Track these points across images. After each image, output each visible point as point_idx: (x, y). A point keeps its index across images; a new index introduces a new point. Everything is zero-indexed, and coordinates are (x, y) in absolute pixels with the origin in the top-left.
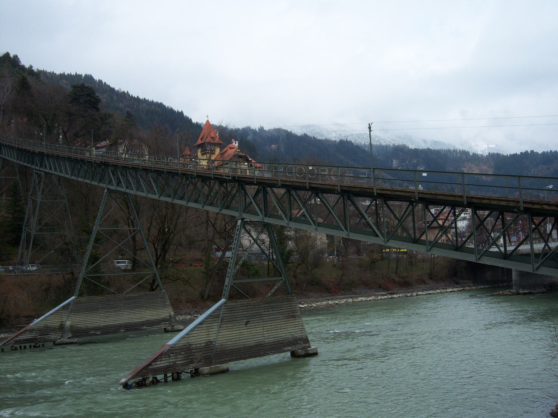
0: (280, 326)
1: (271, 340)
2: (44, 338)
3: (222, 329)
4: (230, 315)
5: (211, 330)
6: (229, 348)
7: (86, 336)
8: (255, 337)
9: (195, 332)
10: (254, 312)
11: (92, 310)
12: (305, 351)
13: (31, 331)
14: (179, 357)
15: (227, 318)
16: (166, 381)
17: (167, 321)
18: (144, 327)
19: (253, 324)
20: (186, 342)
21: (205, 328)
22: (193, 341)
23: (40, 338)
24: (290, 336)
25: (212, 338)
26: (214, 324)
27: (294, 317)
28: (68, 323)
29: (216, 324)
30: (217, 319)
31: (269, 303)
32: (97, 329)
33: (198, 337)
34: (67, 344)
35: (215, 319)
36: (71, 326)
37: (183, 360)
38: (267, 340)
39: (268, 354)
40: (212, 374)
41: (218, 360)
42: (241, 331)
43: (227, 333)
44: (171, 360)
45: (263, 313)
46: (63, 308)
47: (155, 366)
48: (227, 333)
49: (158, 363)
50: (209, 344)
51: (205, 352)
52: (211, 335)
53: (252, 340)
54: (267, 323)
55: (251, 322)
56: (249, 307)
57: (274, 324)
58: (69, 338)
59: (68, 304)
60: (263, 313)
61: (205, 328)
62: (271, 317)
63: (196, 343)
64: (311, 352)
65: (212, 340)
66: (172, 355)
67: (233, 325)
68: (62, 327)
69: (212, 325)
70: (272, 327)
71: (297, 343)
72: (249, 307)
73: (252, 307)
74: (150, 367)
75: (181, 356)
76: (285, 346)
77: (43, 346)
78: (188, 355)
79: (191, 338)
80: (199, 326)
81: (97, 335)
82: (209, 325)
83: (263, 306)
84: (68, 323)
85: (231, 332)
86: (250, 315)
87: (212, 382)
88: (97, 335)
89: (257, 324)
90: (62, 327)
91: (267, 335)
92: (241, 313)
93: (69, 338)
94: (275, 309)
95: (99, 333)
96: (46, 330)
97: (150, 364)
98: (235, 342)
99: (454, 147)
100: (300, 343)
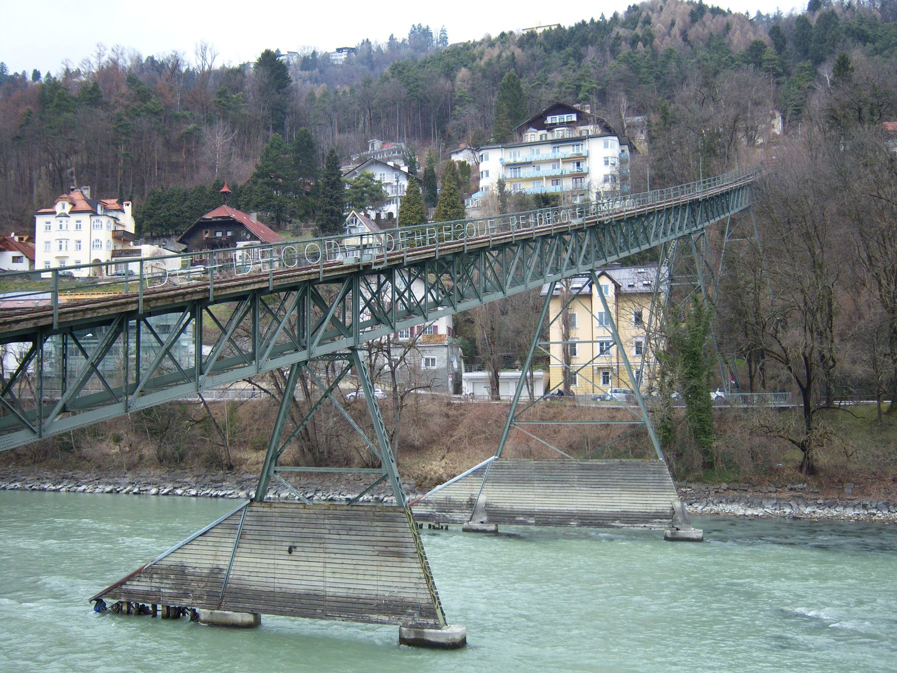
0: (364, 567)
1: (342, 592)
2: (444, 516)
3: (242, 550)
4: (259, 528)
5: (220, 549)
6: (253, 588)
7: (511, 523)
8: (305, 578)
9: (194, 547)
10: (305, 530)
11: (523, 480)
12: (416, 633)
13: (427, 503)
14: (166, 581)
15: (252, 532)
16: (154, 615)
17: (666, 517)
18: (617, 523)
19: (303, 554)
20: (178, 560)
21: (210, 544)
22: (189, 561)
23: (439, 516)
24: (387, 594)
25: (223, 563)
26: (227, 540)
27: (399, 555)
28: (482, 499)
29: (231, 540)
30: (233, 531)
31: (340, 519)
32: (530, 514)
33: (199, 557)
34: (477, 531)
35: (229, 531)
36: (487, 504)
37: (171, 588)
38: (331, 590)
39: (333, 617)
40: (214, 624)
41: (232, 604)
42: (277, 562)
43: (252, 560)
44: (153, 584)
45: (327, 536)
46: (475, 473)
47: (130, 587)
48: (252, 560)
49: (135, 583)
50: (216, 571)
51: (209, 584)
52: (221, 558)
53: (298, 582)
54: (333, 556)
55: (298, 549)
56: (296, 520)
57: (350, 562)
58: (482, 522)
59: (483, 468)
60: (327, 536)
61: (210, 544)
62: (343, 547)
63: (194, 565)
64: (431, 639)
65: (221, 567)
66: (155, 576)
67: (263, 547)
68: (471, 504)
69: (223, 540)
70: (345, 566)
71: (403, 613)
72: (296, 520)
73: (303, 520)
74: (124, 587)
75: (169, 582)
76: (372, 611)
77: (447, 529)
78: (180, 582)
79: (186, 556)
80: (200, 538)
81: (530, 524)
82: (218, 539)
83: (326, 521)
84: (482, 499)
85: (259, 560)
86: (299, 535)
87: (206, 636)
88: (530, 524)
89: (311, 554)
90: (471, 504)
91: (332, 580)
92: (280, 529)
93: (482, 522)
94: (354, 533)
95: (532, 521)
96: (448, 505)
97: (122, 583)
98: (265, 580)
99: (134, 50)
100: (410, 614)
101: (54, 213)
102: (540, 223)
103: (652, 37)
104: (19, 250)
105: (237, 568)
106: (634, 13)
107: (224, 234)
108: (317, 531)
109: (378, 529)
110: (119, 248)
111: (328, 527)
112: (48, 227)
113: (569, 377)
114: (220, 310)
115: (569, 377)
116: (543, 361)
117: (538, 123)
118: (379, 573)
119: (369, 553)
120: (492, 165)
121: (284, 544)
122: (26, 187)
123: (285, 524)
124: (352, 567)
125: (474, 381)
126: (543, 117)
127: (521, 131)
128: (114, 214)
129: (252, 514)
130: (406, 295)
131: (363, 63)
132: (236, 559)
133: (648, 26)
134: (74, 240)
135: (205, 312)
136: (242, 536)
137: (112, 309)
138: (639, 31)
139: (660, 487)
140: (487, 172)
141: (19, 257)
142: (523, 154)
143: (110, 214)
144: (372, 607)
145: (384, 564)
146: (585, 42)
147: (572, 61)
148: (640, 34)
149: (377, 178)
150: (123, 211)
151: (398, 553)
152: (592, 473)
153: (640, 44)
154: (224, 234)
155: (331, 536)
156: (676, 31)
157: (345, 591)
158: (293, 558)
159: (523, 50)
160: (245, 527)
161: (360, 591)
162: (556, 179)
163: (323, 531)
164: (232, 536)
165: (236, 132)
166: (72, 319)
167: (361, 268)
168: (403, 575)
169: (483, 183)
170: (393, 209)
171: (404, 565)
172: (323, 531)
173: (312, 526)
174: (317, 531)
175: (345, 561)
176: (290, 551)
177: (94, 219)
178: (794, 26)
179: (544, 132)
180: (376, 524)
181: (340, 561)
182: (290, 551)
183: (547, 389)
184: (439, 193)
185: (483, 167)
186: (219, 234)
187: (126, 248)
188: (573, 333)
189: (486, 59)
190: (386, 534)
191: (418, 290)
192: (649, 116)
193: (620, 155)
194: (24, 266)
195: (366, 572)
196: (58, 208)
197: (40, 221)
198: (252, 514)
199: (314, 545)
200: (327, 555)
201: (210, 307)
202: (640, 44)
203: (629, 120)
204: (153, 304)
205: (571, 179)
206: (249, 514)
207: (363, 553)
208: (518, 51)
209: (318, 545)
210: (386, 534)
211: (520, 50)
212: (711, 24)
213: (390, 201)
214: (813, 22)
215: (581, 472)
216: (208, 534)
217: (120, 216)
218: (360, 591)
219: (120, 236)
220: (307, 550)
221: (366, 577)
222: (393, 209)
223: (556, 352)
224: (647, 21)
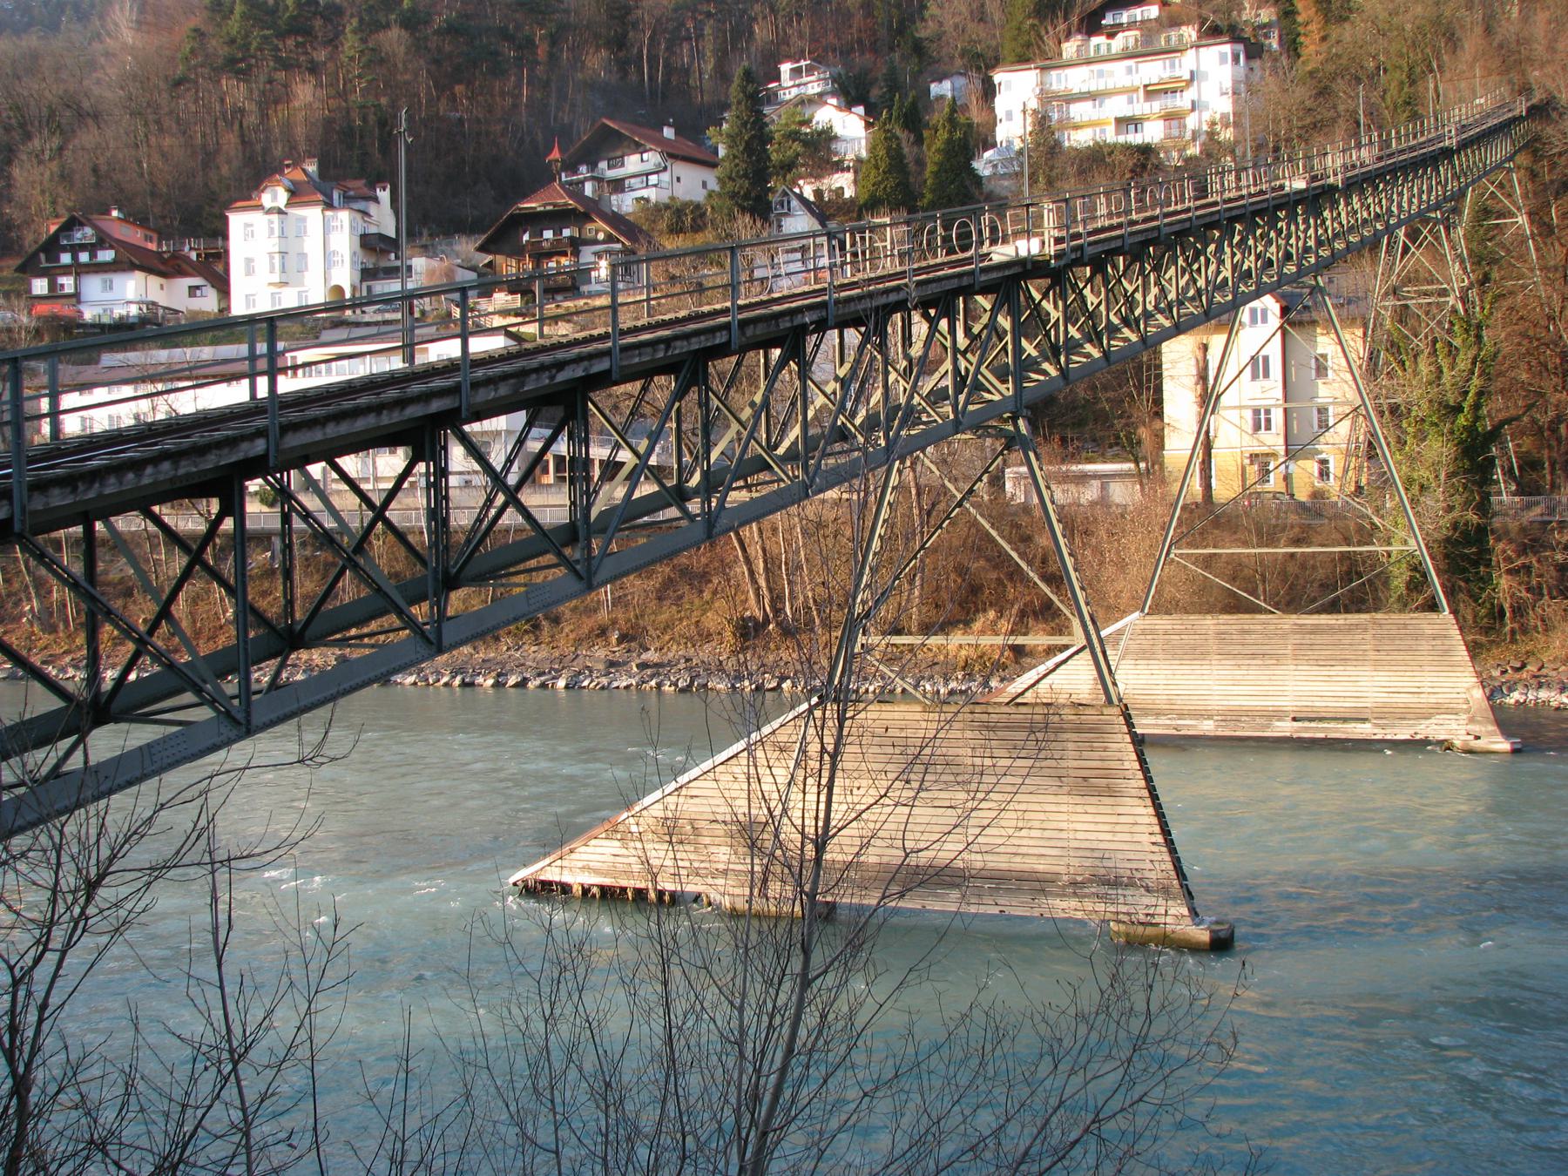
0: (1042, 816)
9: (938, 828)
101: (260, 207)
107: (558, 232)
118: (1072, 826)
126: (1099, 14)
128: (361, 205)
137: (694, 340)
139: (1443, 657)
141: (198, 287)
143: (357, 206)
145: (1079, 809)
150: (376, 200)
152: (1318, 639)
154: (558, 232)
162: (1123, 123)
166: (637, 360)
167: (1029, 267)
168: (1118, 828)
171: (1121, 810)
177: (329, 213)
186: (548, 234)
187: (383, 264)
193: (1247, 76)
194: (208, 302)
195: (1045, 825)
196: (267, 199)
197: (237, 221)
204: (749, 331)
205: (1161, 122)
213: (839, 167)
217: (373, 208)
219: (370, 243)
221: (1047, 834)
222: (844, 183)
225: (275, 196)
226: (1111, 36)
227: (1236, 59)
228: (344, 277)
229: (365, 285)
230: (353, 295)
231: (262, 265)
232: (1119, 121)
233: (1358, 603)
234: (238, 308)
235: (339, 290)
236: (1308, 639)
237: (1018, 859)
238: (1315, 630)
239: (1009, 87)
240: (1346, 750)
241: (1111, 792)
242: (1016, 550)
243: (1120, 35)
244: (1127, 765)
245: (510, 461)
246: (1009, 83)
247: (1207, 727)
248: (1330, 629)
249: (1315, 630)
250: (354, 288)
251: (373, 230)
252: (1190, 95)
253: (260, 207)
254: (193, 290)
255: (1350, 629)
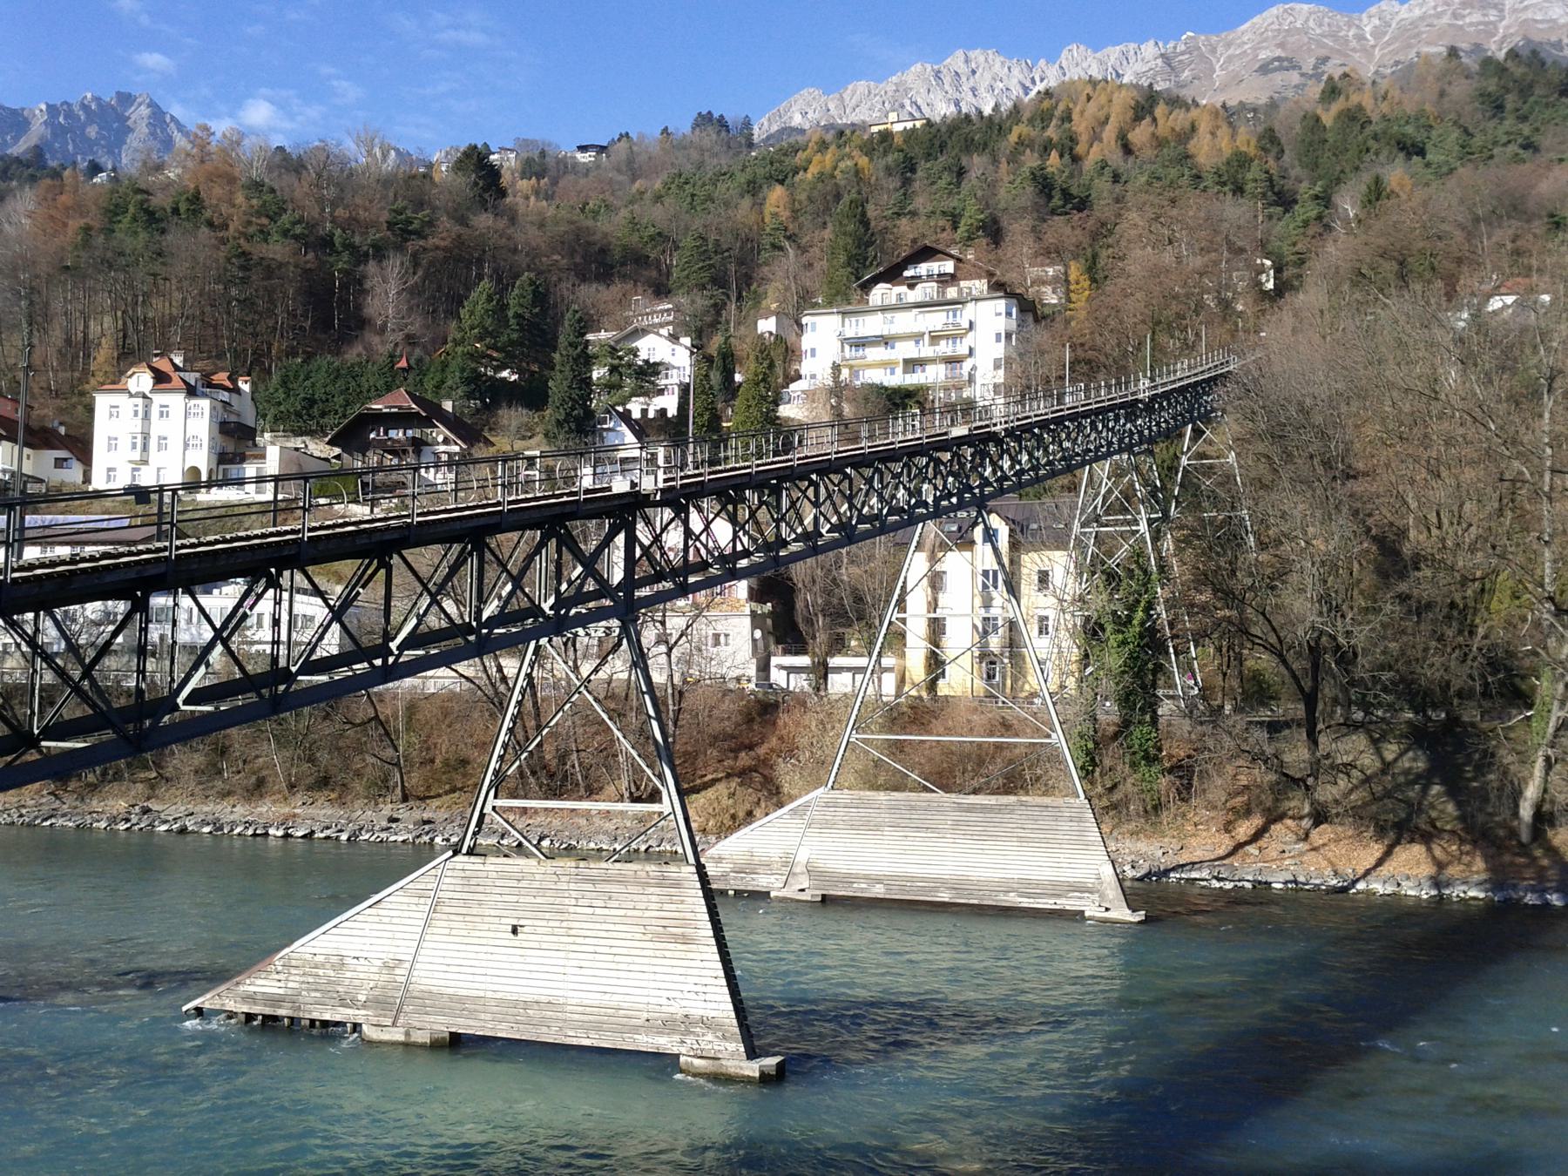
3: (435, 930)
10: (539, 900)
15: (454, 903)
30: (422, 900)
35: (416, 900)
38: (575, 994)
45: (572, 909)
62: (598, 926)
73: (536, 884)
83: (572, 886)
101: (126, 390)
102: (905, 431)
103: (1073, 140)
104: (67, 448)
105: (422, 974)
106: (1046, 104)
108: (558, 901)
109: (654, 898)
110: (230, 448)
111: (574, 894)
112: (114, 411)
113: (936, 664)
114: (426, 558)
115: (936, 664)
116: (897, 638)
117: (892, 275)
119: (639, 936)
120: (823, 341)
121: (504, 920)
122: (78, 350)
123: (507, 891)
124: (610, 958)
125: (791, 670)
127: (866, 287)
129: (456, 873)
130: (703, 538)
131: (619, 171)
132: (429, 931)
133: (1067, 125)
134: (148, 435)
135: (396, 560)
136: (434, 908)
138: (1052, 132)
140: (813, 351)
142: (871, 325)
144: (639, 1022)
146: (969, 146)
147: (946, 177)
148: (1055, 138)
149: (643, 355)
151: (683, 935)
152: (973, 817)
153: (1054, 154)
155: (579, 910)
156: (1109, 133)
157: (598, 996)
158: (517, 944)
159: (871, 160)
160: (441, 894)
161: (620, 998)
162: (911, 364)
163: (567, 901)
164: (421, 908)
165: (420, 273)
169: (806, 367)
170: (669, 403)
172: (567, 901)
173: (550, 893)
174: (558, 901)
175: (598, 949)
176: (515, 931)
178: (1298, 127)
179: (904, 289)
180: (652, 890)
181: (591, 949)
182: (515, 931)
183: (902, 681)
184: (739, 383)
185: (807, 342)
188: (943, 599)
189: (813, 170)
190: (666, 907)
191: (722, 531)
192: (1067, 266)
197: (102, 402)
198: (456, 873)
199: (551, 924)
200: (571, 940)
201: (405, 552)
202: (1054, 154)
203: (1034, 272)
206: (449, 873)
207: (629, 936)
208: (863, 161)
209: (557, 924)
210: (666, 907)
211: (866, 159)
212: (1168, 121)
214: (1328, 119)
215: (957, 816)
216: (383, 905)
218: (620, 998)
220: (539, 930)
223: (916, 629)
224: (1067, 117)
225: (141, 380)
226: (911, 287)
227: (1009, 314)
228: (201, 459)
229: (221, 467)
230: (210, 477)
231: (125, 443)
232: (906, 361)
233: (1012, 783)
234: (98, 482)
235: (195, 471)
236: (965, 816)
237: (607, 997)
238: (971, 809)
239: (814, 329)
240: (844, 906)
241: (685, 940)
242: (899, 762)
243: (919, 286)
244: (699, 916)
245: (500, 669)
246: (814, 324)
247: (878, 891)
248: (984, 809)
249: (971, 809)
250: (210, 472)
251: (233, 418)
252: (969, 340)
253: (126, 390)
254: (59, 463)
255: (999, 809)
